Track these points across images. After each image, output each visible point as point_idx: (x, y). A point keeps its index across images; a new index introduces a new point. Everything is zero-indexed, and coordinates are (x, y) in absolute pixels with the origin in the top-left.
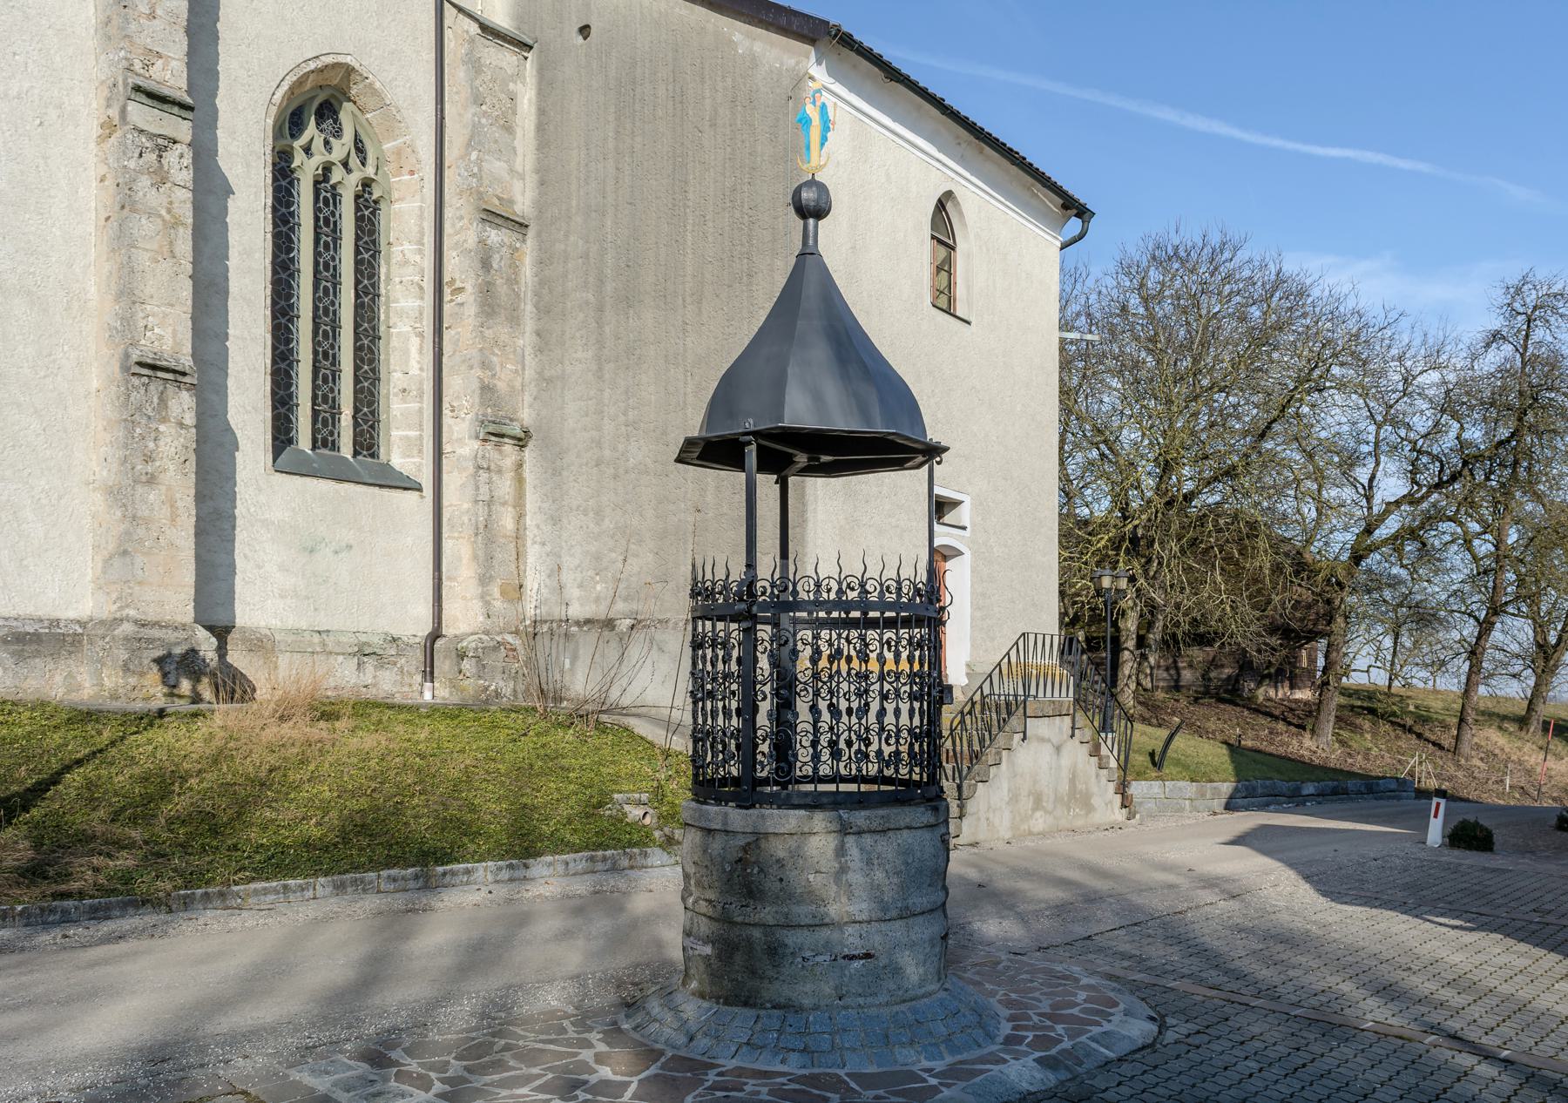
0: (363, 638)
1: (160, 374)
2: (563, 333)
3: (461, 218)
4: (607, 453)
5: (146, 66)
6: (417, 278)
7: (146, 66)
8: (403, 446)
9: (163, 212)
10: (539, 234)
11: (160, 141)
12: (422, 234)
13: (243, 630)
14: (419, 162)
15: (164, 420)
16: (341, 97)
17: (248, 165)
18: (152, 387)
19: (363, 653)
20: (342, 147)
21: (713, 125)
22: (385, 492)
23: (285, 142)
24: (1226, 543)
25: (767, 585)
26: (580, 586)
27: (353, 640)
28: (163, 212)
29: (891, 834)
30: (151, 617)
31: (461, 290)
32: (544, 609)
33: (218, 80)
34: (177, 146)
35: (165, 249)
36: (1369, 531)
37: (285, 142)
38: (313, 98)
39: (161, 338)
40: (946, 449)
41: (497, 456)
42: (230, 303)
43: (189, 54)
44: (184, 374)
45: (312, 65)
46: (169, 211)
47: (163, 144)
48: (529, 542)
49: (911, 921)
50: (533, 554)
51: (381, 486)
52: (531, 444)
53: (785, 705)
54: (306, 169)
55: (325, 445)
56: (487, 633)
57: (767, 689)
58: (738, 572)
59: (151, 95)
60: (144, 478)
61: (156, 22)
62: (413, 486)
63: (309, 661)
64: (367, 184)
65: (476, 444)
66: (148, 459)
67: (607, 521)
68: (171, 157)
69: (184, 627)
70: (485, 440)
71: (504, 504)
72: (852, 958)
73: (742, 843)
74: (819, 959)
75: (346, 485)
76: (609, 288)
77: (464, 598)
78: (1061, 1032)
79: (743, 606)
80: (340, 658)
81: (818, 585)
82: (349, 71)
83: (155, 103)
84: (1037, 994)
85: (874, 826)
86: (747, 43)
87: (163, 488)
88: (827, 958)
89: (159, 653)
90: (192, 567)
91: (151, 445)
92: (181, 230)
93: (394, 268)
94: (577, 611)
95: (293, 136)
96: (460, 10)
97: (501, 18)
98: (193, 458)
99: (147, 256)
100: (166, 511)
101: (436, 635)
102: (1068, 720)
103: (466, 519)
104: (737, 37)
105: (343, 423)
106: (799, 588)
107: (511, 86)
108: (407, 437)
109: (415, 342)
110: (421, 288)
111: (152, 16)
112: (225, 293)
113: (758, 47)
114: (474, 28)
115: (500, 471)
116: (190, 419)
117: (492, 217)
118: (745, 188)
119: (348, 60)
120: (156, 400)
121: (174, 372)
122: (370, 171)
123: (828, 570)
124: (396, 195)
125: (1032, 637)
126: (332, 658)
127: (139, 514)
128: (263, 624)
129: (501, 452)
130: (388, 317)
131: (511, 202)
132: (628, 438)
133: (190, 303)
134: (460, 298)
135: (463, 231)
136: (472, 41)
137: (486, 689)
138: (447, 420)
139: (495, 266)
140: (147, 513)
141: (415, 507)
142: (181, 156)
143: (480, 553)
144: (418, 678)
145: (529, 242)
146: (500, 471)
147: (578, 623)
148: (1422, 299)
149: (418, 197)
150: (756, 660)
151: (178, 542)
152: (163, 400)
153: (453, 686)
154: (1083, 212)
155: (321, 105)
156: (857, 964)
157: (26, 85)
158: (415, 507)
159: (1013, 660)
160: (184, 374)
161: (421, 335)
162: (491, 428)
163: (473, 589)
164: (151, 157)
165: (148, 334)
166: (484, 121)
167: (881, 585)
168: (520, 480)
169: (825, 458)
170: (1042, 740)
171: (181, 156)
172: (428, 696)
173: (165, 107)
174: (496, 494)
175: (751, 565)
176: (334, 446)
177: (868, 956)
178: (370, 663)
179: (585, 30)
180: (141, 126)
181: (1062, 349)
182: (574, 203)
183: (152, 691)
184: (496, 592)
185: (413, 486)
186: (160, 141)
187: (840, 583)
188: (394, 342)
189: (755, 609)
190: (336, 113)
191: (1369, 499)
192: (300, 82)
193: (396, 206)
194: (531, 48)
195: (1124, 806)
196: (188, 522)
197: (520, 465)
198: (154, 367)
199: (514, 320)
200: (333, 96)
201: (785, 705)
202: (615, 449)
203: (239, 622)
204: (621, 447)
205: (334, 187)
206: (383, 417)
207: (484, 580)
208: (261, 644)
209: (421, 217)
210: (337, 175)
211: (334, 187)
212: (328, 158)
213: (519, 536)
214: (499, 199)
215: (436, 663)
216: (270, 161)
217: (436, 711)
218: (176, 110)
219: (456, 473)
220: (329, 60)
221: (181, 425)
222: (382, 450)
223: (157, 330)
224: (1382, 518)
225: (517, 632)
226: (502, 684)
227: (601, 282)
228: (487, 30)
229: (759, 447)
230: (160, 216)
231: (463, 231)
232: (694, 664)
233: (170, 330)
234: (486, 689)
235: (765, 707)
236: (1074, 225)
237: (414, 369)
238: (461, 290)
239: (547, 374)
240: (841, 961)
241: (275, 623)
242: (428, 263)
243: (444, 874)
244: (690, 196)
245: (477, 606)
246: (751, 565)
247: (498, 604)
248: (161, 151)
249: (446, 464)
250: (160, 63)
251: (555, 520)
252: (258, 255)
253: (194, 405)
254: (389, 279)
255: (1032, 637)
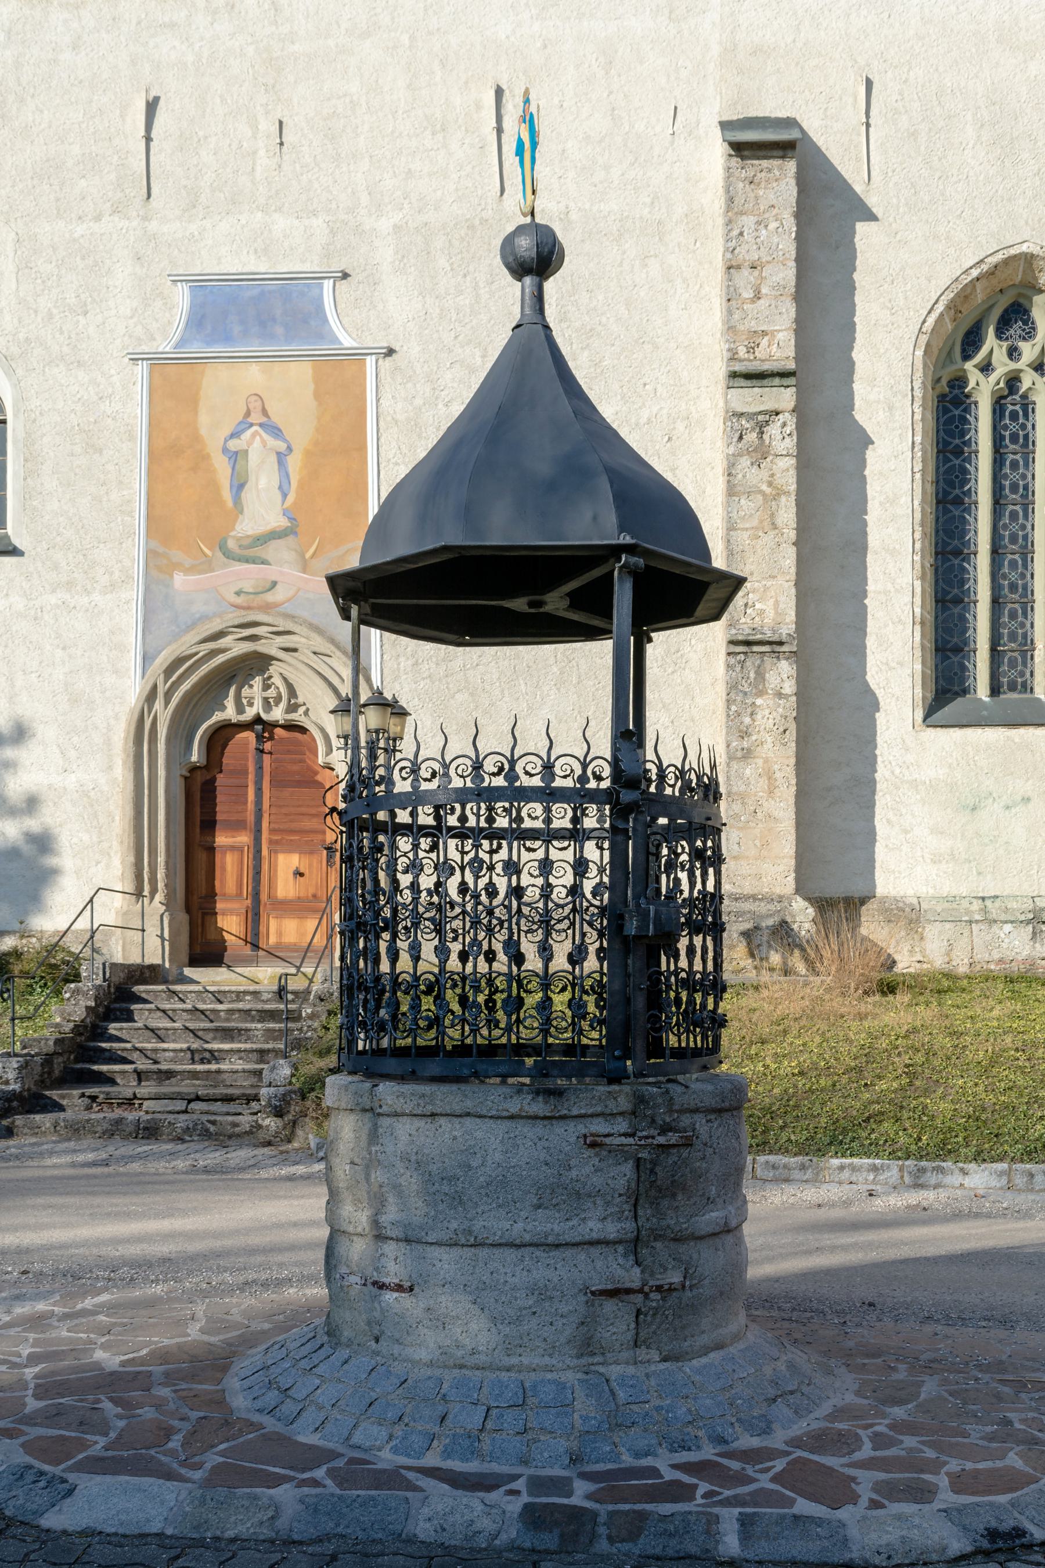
1: (755, 649)
5: (751, 350)
7: (751, 350)
9: (764, 487)
11: (760, 418)
13: (884, 899)
15: (761, 693)
16: (1029, 293)
17: (891, 408)
18: (748, 663)
23: (954, 367)
28: (764, 487)
30: (748, 890)
33: (854, 331)
34: (780, 416)
35: (766, 524)
37: (954, 367)
39: (761, 613)
42: (870, 558)
43: (797, 321)
44: (781, 643)
45: (975, 273)
46: (770, 484)
47: (762, 421)
54: (983, 391)
55: (1012, 687)
59: (749, 376)
60: (739, 754)
61: (762, 301)
63: (966, 933)
66: (744, 734)
68: (773, 430)
69: (780, 899)
75: (1022, 731)
80: (1008, 927)
82: (1029, 259)
83: (755, 382)
87: (760, 762)
89: (748, 926)
90: (792, 837)
91: (747, 720)
92: (783, 499)
95: (966, 357)
98: (793, 727)
99: (745, 535)
100: (763, 783)
111: (757, 296)
112: (864, 548)
116: (789, 687)
119: (1024, 248)
120: (752, 675)
121: (770, 643)
123: (671, 756)
126: (995, 928)
127: (735, 789)
128: (910, 892)
133: (793, 570)
140: (743, 788)
142: (784, 425)
151: (776, 814)
152: (760, 675)
155: (1006, 311)
157: (655, 409)
160: (781, 643)
164: (752, 437)
165: (749, 611)
171: (784, 425)
173: (765, 382)
180: (740, 409)
183: (742, 964)
186: (760, 418)
190: (1026, 312)
196: (787, 792)
198: (748, 643)
200: (1020, 295)
203: (880, 891)
205: (1025, 396)
208: (909, 917)
211: (1025, 396)
212: (1013, 366)
218: (777, 381)
221: (779, 695)
223: (758, 606)
230: (761, 492)
233: (772, 602)
241: (924, 890)
243: (842, 1168)
248: (761, 429)
250: (764, 342)
252: (906, 500)
253: (794, 673)
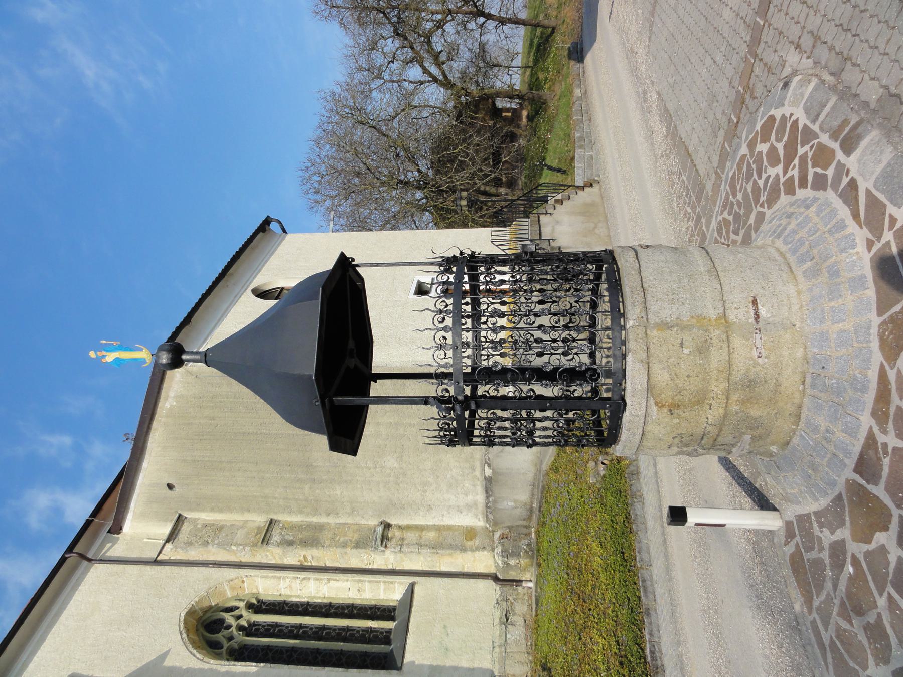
0: (497, 621)
2: (326, 501)
3: (267, 555)
4: (392, 479)
6: (299, 581)
8: (389, 593)
10: (276, 513)
12: (275, 577)
14: (237, 578)
19: (506, 620)
20: (229, 618)
21: (213, 419)
22: (415, 604)
24: (445, 156)
25: (440, 388)
26: (466, 495)
27: (498, 627)
29: (645, 286)
31: (305, 557)
32: (480, 516)
36: (435, 80)
38: (203, 635)
40: (342, 254)
41: (394, 540)
45: (184, 636)
48: (442, 523)
49: (719, 269)
50: (448, 521)
51: (411, 607)
52: (389, 521)
53: (540, 374)
54: (240, 638)
56: (493, 550)
57: (525, 388)
58: (433, 411)
62: (412, 585)
64: (250, 606)
65: (388, 552)
67: (430, 480)
70: (386, 547)
71: (421, 537)
72: (757, 316)
73: (654, 409)
74: (759, 344)
76: (302, 476)
77: (474, 561)
78: (807, 148)
79: (458, 407)
81: (441, 347)
84: (761, 183)
85: (640, 298)
86: (170, 400)
88: (758, 336)
93: (294, 594)
94: (480, 498)
96: (160, 552)
97: (167, 530)
101: (496, 579)
102: (542, 217)
103: (429, 559)
104: (167, 405)
105: (376, 626)
106: (443, 362)
107: (199, 526)
108: (384, 590)
109: (332, 583)
110: (304, 579)
113: (172, 394)
114: (169, 546)
115: (403, 539)
117: (266, 540)
118: (245, 400)
119: (183, 615)
122: (242, 605)
124: (255, 591)
125: (493, 238)
129: (392, 538)
130: (319, 598)
131: (259, 528)
132: (382, 467)
134: (309, 558)
135: (273, 554)
136: (176, 547)
137: (526, 551)
138: (375, 566)
139: (291, 538)
141: (423, 587)
143: (448, 552)
144: (520, 589)
145: (280, 518)
146: (403, 539)
147: (487, 498)
148: (319, 59)
149: (256, 579)
150: (504, 397)
153: (524, 570)
154: (267, 222)
156: (763, 312)
158: (423, 587)
159: (507, 247)
161: (329, 580)
162: (379, 543)
163: (469, 555)
166: (216, 542)
167: (440, 297)
168: (408, 527)
169: (351, 344)
170: (553, 230)
172: (531, 585)
174: (415, 542)
175: (426, 401)
176: (389, 632)
177: (755, 302)
178: (511, 618)
179: (170, 487)
181: (337, 231)
182: (258, 494)
184: (469, 543)
185: (412, 585)
187: (439, 330)
188: (332, 595)
189: (460, 398)
191: (422, 83)
192: (193, 643)
193: (261, 591)
194: (180, 515)
195: (591, 185)
197: (400, 527)
199: (320, 527)
201: (540, 374)
202: (389, 475)
204: (388, 471)
206: (373, 603)
207: (463, 549)
209: (266, 577)
210: (243, 623)
213: (438, 528)
214: (257, 534)
215: (511, 578)
216: (233, 663)
217: (540, 580)
219: (404, 563)
220: (182, 625)
222: (391, 604)
224: (430, 74)
225: (493, 531)
226: (523, 542)
227: (299, 480)
228: (170, 538)
229: (336, 395)
231: (273, 554)
232: (507, 444)
234: (526, 551)
235: (540, 389)
236: (274, 226)
237: (347, 584)
238: (305, 557)
239: (349, 510)
240: (760, 325)
242: (291, 574)
244: (251, 431)
245: (478, 554)
246: (426, 401)
247: (477, 542)
249: (399, 567)
251: (430, 508)
254: (298, 596)
255: (493, 238)
